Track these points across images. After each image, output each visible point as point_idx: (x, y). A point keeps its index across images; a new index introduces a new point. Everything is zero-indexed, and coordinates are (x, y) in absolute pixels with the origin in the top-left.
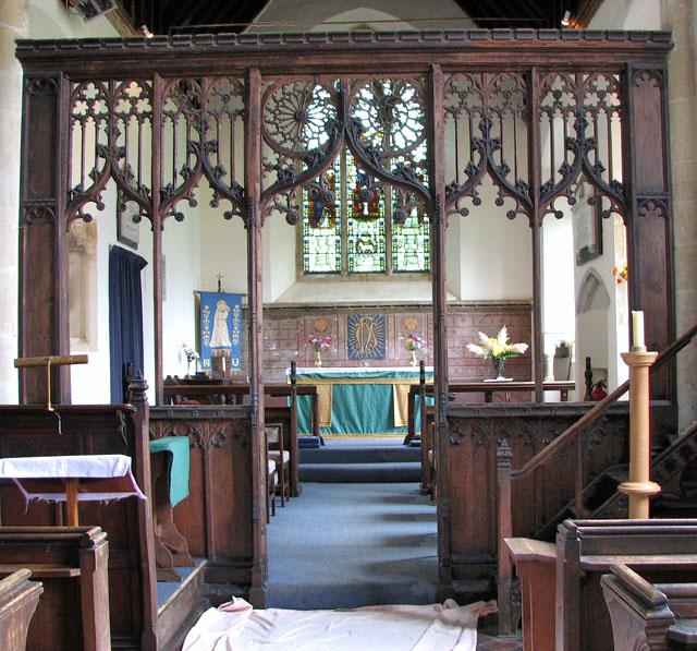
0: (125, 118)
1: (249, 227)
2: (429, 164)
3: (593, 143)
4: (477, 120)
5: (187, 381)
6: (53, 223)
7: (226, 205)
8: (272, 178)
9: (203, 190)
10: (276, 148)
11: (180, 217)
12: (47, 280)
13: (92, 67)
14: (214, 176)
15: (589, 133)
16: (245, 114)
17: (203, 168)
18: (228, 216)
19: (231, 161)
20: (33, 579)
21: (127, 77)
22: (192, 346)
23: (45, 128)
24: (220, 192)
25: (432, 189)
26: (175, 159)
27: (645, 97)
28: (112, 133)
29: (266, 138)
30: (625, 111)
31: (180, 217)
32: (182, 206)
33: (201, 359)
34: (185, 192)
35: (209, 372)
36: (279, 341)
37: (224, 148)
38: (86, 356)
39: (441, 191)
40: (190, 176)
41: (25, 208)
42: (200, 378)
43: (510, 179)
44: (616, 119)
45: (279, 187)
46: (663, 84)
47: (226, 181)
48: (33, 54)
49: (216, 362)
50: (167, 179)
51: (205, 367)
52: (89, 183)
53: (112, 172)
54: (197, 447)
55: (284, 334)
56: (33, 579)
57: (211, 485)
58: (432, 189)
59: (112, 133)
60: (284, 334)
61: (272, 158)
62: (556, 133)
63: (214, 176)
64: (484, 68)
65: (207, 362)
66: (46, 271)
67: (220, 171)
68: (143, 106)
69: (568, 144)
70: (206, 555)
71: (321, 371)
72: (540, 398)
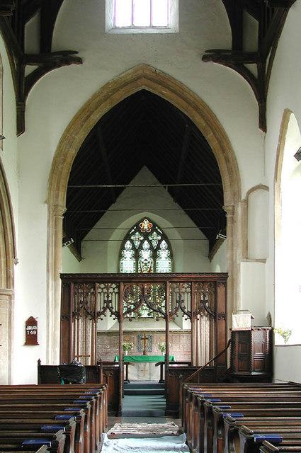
0: (184, 293)
1: (119, 322)
2: (166, 306)
3: (111, 301)
4: (106, 295)
6: (69, 320)
7: (114, 316)
9: (108, 313)
11: (102, 319)
12: (67, 335)
17: (108, 307)
18: (186, 319)
24: (112, 313)
25: (166, 313)
28: (108, 297)
31: (102, 319)
32: (102, 316)
34: (103, 313)
36: (110, 344)
37: (185, 301)
38: (36, 344)
39: (168, 314)
41: (62, 317)
43: (186, 310)
45: (126, 313)
46: (226, 286)
47: (114, 310)
50: (98, 310)
52: (102, 310)
53: (108, 307)
55: (113, 342)
58: (166, 313)
60: (113, 342)
64: (180, 282)
66: (67, 333)
69: (105, 302)
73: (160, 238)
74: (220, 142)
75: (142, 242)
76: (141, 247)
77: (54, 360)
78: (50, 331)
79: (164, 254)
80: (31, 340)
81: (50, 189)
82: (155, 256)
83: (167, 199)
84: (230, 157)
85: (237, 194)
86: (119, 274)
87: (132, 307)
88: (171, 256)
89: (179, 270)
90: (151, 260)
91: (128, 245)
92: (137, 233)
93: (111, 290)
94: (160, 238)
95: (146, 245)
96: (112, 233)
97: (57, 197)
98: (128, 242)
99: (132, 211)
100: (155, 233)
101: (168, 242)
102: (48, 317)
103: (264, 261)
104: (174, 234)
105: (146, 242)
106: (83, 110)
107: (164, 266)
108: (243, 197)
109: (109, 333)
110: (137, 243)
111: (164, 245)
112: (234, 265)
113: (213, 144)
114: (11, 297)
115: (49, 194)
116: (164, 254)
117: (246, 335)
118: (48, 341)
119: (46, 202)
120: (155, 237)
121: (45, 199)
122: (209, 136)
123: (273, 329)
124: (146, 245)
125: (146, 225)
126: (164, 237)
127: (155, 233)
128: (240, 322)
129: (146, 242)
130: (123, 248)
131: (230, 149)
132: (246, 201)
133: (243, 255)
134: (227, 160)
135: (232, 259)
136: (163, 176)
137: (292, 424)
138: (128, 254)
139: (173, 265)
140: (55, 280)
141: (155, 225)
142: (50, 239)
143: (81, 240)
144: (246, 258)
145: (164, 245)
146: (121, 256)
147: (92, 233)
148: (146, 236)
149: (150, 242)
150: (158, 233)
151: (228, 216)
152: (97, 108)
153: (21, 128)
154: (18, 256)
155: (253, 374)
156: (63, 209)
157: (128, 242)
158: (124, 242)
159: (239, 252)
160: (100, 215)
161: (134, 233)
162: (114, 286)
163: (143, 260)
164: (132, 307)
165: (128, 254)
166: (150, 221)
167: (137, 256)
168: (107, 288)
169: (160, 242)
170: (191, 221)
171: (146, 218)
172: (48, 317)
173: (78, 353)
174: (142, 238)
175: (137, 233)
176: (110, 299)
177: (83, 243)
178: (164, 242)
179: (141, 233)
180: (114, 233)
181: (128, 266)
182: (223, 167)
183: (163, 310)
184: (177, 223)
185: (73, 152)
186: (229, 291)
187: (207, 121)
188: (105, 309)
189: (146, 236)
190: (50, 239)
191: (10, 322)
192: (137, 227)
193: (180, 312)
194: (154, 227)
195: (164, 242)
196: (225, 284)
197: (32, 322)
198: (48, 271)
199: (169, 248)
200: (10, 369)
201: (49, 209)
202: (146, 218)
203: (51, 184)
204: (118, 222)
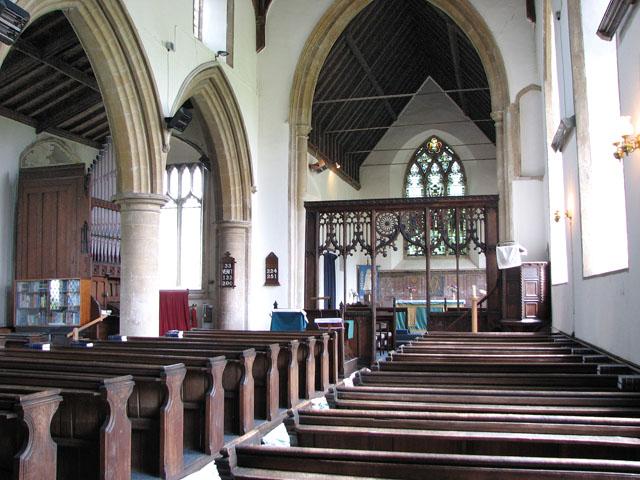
3: (362, 233)
4: (469, 223)
5: (353, 305)
7: (365, 251)
8: (378, 243)
10: (380, 233)
13: (326, 209)
14: (362, 242)
15: (474, 227)
16: (371, 223)
17: (358, 240)
19: (366, 237)
20: (60, 394)
21: (350, 212)
22: (355, 290)
23: (312, 228)
24: (363, 247)
26: (350, 237)
27: (491, 216)
28: (358, 228)
29: (377, 230)
30: (485, 220)
32: (352, 251)
33: (359, 296)
34: (353, 247)
35: (363, 302)
36: (394, 288)
37: (338, 234)
39: (429, 247)
40: (355, 243)
42: (359, 304)
44: (483, 222)
45: (381, 246)
46: (497, 211)
48: (310, 206)
49: (366, 297)
51: (361, 299)
53: (358, 240)
54: (356, 324)
56: (60, 394)
57: (360, 336)
59: (358, 228)
61: (378, 236)
62: (351, 230)
63: (362, 242)
65: (362, 297)
67: (363, 241)
68: (341, 221)
69: (355, 233)
70: (358, 356)
71: (411, 301)
72: (484, 309)
73: (450, 159)
74: (482, 38)
75: (430, 165)
76: (429, 170)
77: (296, 304)
78: (293, 269)
79: (456, 178)
80: (272, 281)
81: (291, 106)
82: (446, 180)
83: (459, 113)
84: (495, 54)
85: (506, 97)
86: (446, 197)
87: (387, 239)
88: (464, 181)
89: (472, 193)
90: (440, 186)
91: (414, 168)
92: (424, 155)
93: (362, 220)
94: (450, 159)
95: (435, 168)
96: (394, 156)
97: (300, 114)
98: (414, 166)
99: (423, 125)
100: (444, 154)
101: (460, 163)
102: (290, 252)
103: (542, 177)
104: (464, 152)
105: (435, 165)
106: (325, 17)
107: (456, 189)
108: (513, 100)
109: (393, 274)
110: (425, 167)
111: (456, 166)
112: (506, 185)
113: (475, 42)
114: (247, 230)
115: (291, 112)
116: (456, 178)
117: (515, 273)
118: (290, 281)
119: (286, 121)
120: (445, 158)
121: (286, 117)
122: (470, 33)
123: (549, 264)
124: (435, 168)
125: (434, 144)
126: (456, 158)
127: (444, 154)
128: (510, 257)
129: (435, 165)
130: (408, 172)
131: (495, 46)
132: (517, 106)
133: (515, 172)
134: (492, 59)
135: (503, 178)
136: (446, 82)
137: (463, 400)
138: (415, 179)
139: (466, 190)
140: (299, 210)
141: (445, 144)
142: (293, 163)
143: (360, 165)
144: (521, 176)
145: (456, 166)
146: (406, 182)
147: (373, 157)
148: (435, 157)
149: (440, 165)
150: (449, 153)
151: (497, 124)
152: (341, 13)
153: (260, 43)
154: (256, 183)
155: (524, 321)
156: (307, 129)
157: (414, 166)
158: (410, 166)
159: (511, 168)
160: (380, 135)
161: (421, 155)
162: (365, 215)
163: (431, 186)
164: (387, 239)
165: (415, 179)
166: (439, 140)
167: (425, 181)
168: (331, 219)
169: (451, 163)
170: (485, 137)
171: (434, 137)
172: (290, 252)
173: (330, 300)
174: (430, 161)
175: (424, 155)
176: (361, 230)
177: (361, 168)
178: (455, 164)
179: (428, 154)
180: (397, 156)
181: (415, 191)
182: (488, 68)
183: (422, 242)
184: (460, 137)
185: (317, 64)
186: (501, 217)
187: (466, 15)
188: (355, 243)
189: (435, 157)
190: (293, 163)
191: (247, 259)
192: (425, 147)
193: (472, 245)
194: (443, 146)
195: (455, 164)
196: (496, 209)
197: (272, 261)
198: (289, 199)
199: (462, 170)
200: (247, 314)
201: (291, 129)
202: (434, 137)
203: (292, 101)
204: (403, 142)
